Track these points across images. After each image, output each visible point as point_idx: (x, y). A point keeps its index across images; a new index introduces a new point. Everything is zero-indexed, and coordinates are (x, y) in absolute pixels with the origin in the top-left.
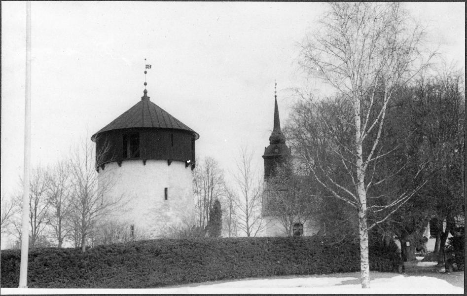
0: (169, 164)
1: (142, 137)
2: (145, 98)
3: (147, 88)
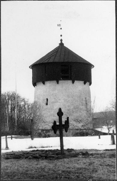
0: (73, 83)
1: (62, 67)
2: (61, 44)
3: (62, 38)
